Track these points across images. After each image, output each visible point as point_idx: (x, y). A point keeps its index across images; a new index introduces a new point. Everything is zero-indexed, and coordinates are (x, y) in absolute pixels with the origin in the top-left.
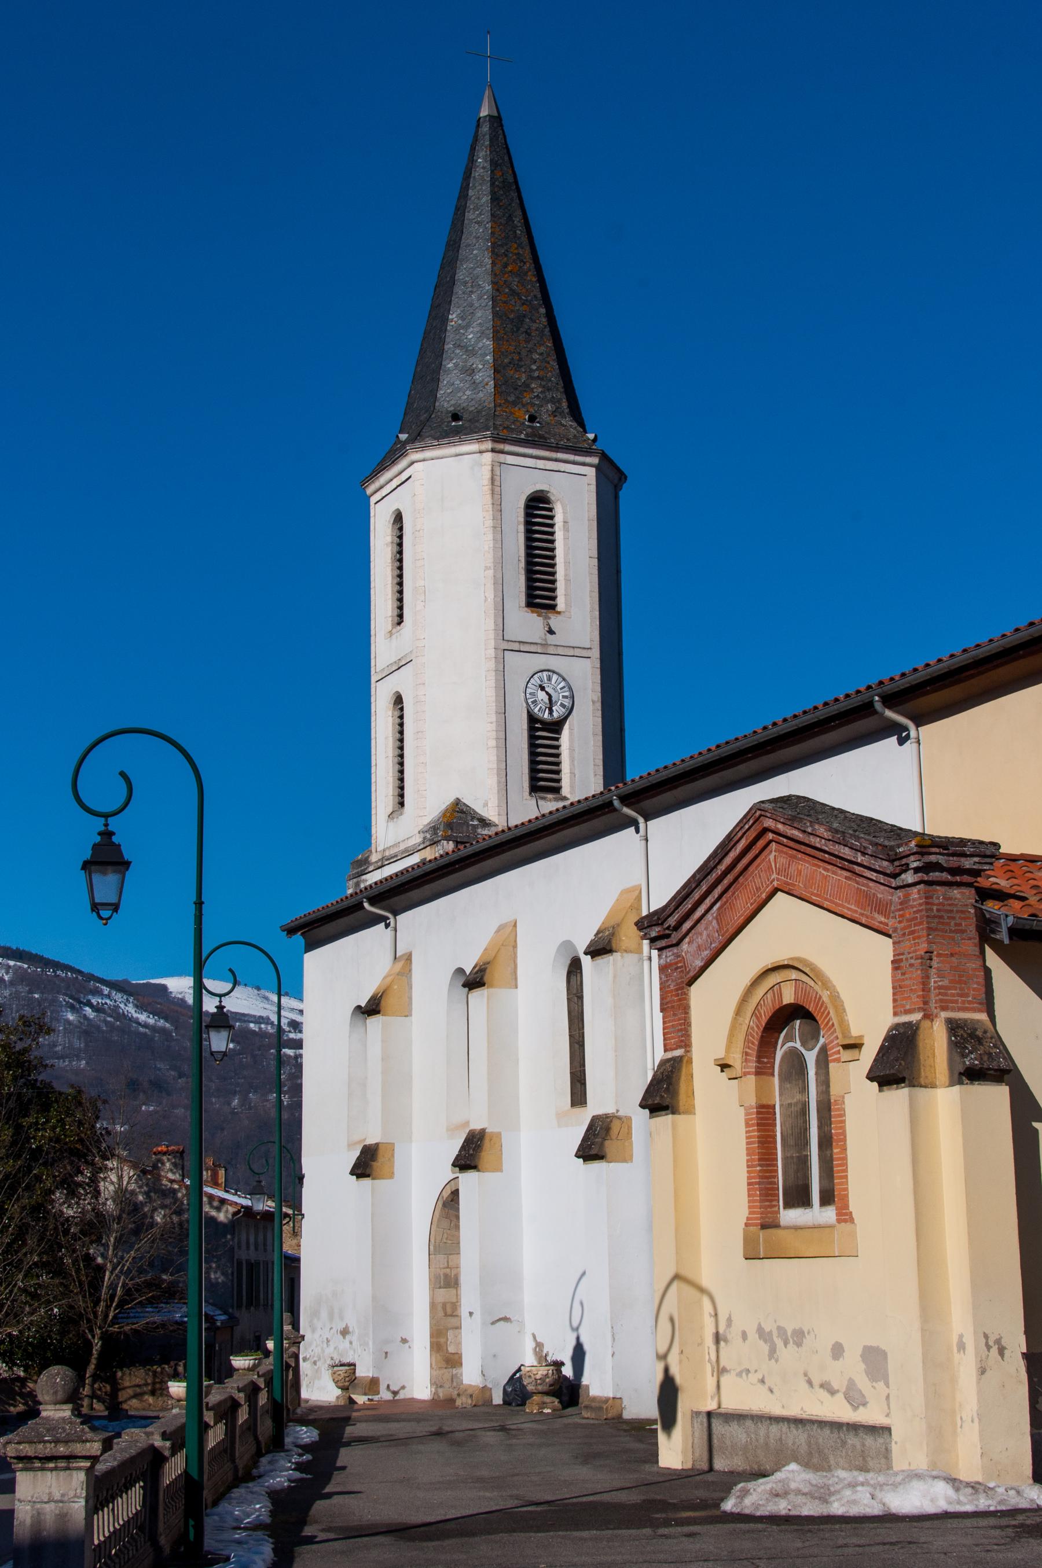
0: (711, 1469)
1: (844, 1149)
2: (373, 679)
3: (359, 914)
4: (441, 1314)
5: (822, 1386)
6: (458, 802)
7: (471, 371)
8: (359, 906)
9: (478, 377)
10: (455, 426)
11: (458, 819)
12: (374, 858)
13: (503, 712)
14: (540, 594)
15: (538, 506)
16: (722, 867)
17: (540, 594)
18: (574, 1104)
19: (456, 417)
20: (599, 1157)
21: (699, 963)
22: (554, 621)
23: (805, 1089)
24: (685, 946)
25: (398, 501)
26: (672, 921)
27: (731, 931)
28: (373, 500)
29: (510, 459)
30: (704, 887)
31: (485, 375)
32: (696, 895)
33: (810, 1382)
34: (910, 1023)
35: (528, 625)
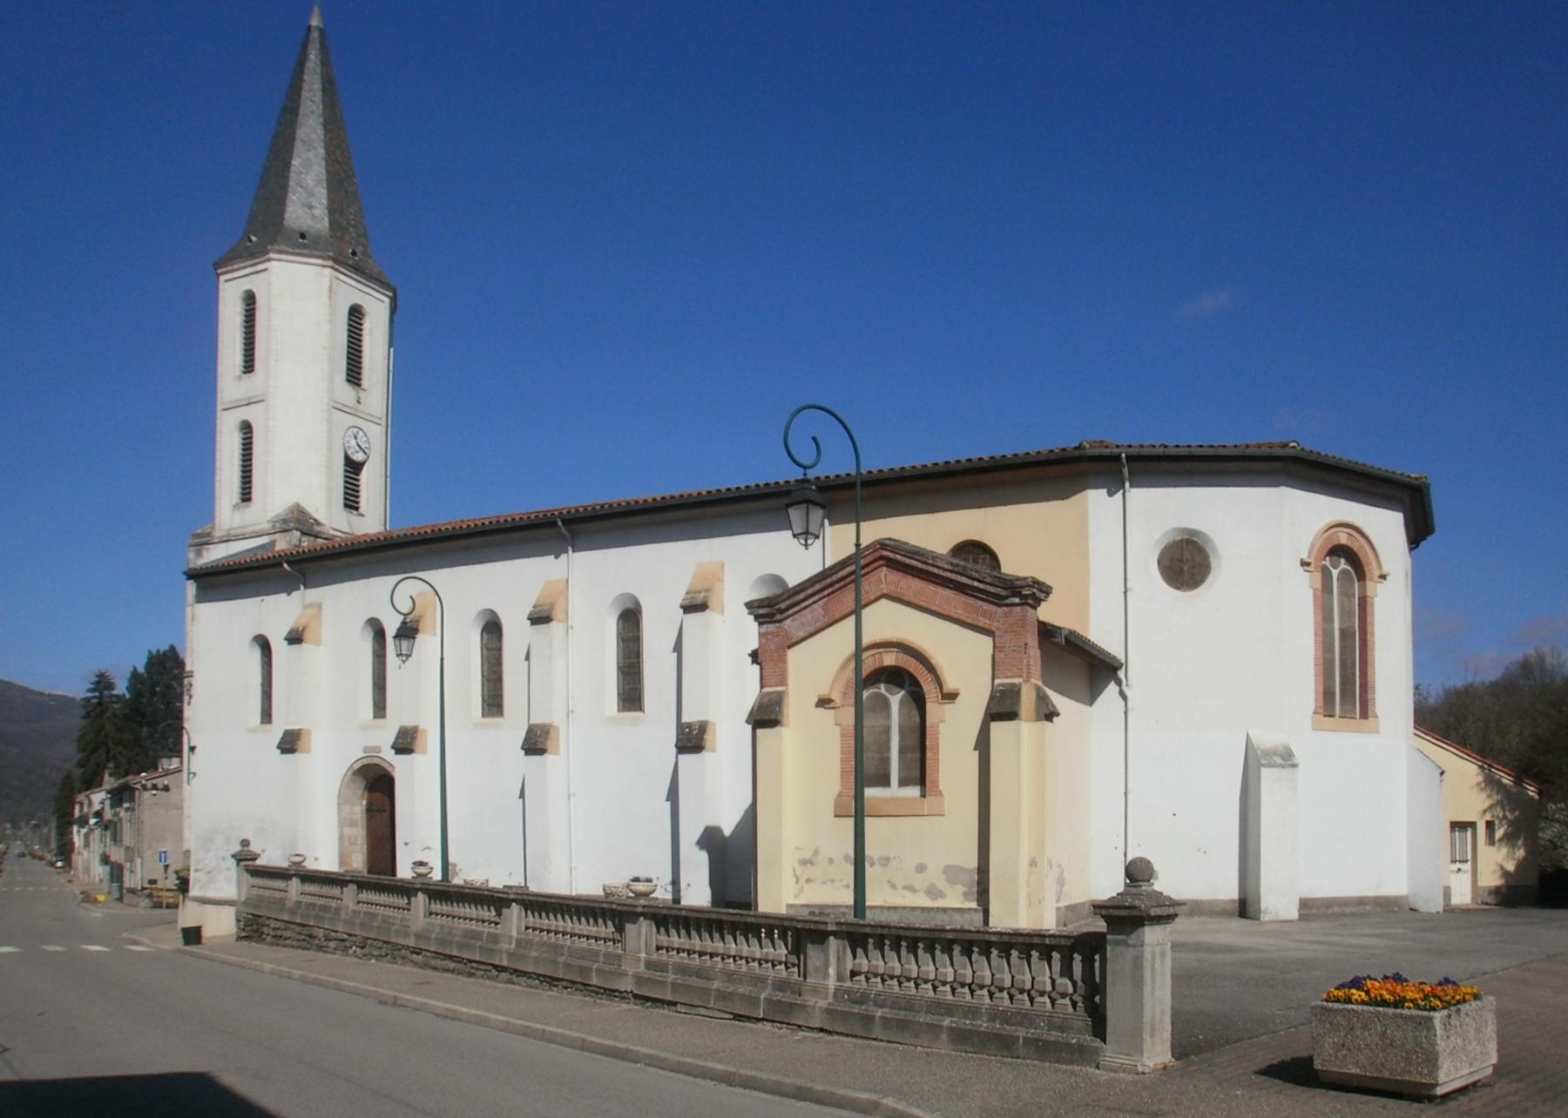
0: (1245, 908)
1: (937, 754)
2: (219, 408)
3: (277, 570)
4: (346, 843)
5: (905, 888)
6: (298, 505)
7: (311, 207)
8: (280, 564)
9: (316, 212)
10: (303, 243)
11: (299, 520)
12: (217, 534)
13: (330, 449)
14: (354, 374)
15: (356, 313)
16: (835, 578)
17: (354, 374)
18: (263, 722)
19: (303, 236)
20: (541, 751)
21: (802, 634)
22: (362, 394)
23: (888, 717)
24: (788, 622)
25: (255, 284)
26: (783, 606)
27: (837, 616)
28: (222, 278)
29: (342, 277)
30: (818, 587)
31: (321, 211)
32: (810, 591)
33: (894, 887)
34: (1014, 685)
35: (346, 393)
